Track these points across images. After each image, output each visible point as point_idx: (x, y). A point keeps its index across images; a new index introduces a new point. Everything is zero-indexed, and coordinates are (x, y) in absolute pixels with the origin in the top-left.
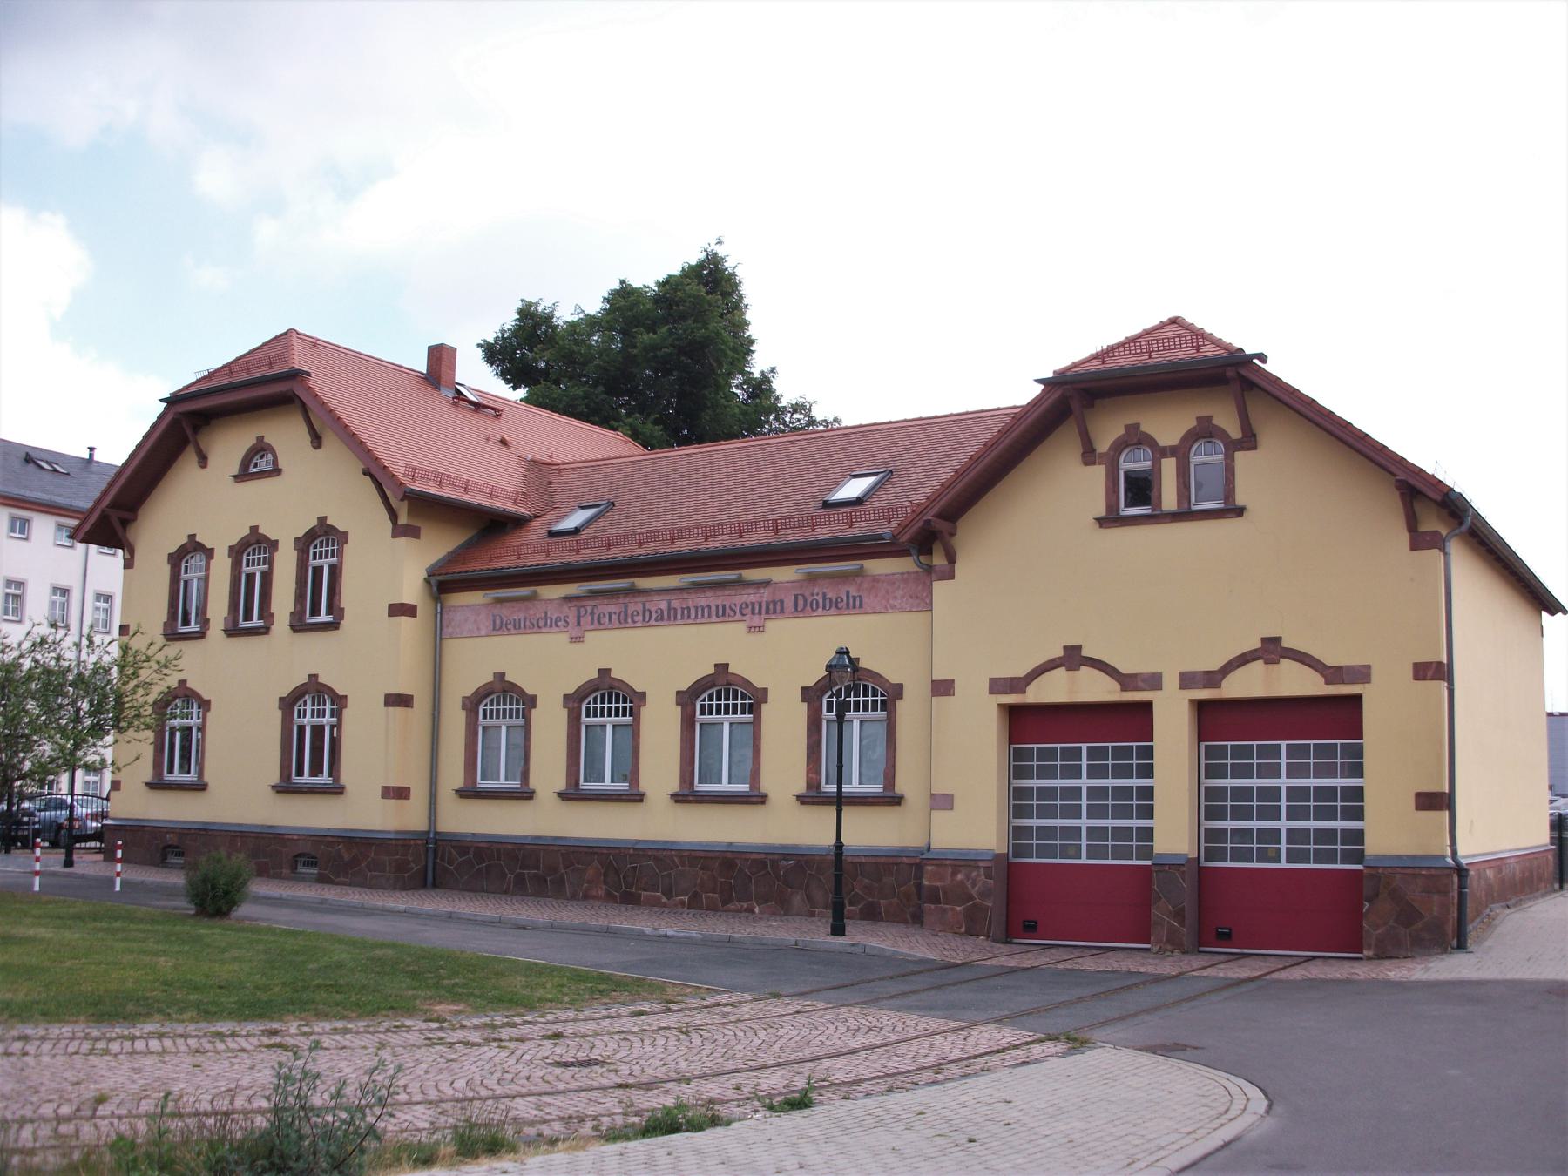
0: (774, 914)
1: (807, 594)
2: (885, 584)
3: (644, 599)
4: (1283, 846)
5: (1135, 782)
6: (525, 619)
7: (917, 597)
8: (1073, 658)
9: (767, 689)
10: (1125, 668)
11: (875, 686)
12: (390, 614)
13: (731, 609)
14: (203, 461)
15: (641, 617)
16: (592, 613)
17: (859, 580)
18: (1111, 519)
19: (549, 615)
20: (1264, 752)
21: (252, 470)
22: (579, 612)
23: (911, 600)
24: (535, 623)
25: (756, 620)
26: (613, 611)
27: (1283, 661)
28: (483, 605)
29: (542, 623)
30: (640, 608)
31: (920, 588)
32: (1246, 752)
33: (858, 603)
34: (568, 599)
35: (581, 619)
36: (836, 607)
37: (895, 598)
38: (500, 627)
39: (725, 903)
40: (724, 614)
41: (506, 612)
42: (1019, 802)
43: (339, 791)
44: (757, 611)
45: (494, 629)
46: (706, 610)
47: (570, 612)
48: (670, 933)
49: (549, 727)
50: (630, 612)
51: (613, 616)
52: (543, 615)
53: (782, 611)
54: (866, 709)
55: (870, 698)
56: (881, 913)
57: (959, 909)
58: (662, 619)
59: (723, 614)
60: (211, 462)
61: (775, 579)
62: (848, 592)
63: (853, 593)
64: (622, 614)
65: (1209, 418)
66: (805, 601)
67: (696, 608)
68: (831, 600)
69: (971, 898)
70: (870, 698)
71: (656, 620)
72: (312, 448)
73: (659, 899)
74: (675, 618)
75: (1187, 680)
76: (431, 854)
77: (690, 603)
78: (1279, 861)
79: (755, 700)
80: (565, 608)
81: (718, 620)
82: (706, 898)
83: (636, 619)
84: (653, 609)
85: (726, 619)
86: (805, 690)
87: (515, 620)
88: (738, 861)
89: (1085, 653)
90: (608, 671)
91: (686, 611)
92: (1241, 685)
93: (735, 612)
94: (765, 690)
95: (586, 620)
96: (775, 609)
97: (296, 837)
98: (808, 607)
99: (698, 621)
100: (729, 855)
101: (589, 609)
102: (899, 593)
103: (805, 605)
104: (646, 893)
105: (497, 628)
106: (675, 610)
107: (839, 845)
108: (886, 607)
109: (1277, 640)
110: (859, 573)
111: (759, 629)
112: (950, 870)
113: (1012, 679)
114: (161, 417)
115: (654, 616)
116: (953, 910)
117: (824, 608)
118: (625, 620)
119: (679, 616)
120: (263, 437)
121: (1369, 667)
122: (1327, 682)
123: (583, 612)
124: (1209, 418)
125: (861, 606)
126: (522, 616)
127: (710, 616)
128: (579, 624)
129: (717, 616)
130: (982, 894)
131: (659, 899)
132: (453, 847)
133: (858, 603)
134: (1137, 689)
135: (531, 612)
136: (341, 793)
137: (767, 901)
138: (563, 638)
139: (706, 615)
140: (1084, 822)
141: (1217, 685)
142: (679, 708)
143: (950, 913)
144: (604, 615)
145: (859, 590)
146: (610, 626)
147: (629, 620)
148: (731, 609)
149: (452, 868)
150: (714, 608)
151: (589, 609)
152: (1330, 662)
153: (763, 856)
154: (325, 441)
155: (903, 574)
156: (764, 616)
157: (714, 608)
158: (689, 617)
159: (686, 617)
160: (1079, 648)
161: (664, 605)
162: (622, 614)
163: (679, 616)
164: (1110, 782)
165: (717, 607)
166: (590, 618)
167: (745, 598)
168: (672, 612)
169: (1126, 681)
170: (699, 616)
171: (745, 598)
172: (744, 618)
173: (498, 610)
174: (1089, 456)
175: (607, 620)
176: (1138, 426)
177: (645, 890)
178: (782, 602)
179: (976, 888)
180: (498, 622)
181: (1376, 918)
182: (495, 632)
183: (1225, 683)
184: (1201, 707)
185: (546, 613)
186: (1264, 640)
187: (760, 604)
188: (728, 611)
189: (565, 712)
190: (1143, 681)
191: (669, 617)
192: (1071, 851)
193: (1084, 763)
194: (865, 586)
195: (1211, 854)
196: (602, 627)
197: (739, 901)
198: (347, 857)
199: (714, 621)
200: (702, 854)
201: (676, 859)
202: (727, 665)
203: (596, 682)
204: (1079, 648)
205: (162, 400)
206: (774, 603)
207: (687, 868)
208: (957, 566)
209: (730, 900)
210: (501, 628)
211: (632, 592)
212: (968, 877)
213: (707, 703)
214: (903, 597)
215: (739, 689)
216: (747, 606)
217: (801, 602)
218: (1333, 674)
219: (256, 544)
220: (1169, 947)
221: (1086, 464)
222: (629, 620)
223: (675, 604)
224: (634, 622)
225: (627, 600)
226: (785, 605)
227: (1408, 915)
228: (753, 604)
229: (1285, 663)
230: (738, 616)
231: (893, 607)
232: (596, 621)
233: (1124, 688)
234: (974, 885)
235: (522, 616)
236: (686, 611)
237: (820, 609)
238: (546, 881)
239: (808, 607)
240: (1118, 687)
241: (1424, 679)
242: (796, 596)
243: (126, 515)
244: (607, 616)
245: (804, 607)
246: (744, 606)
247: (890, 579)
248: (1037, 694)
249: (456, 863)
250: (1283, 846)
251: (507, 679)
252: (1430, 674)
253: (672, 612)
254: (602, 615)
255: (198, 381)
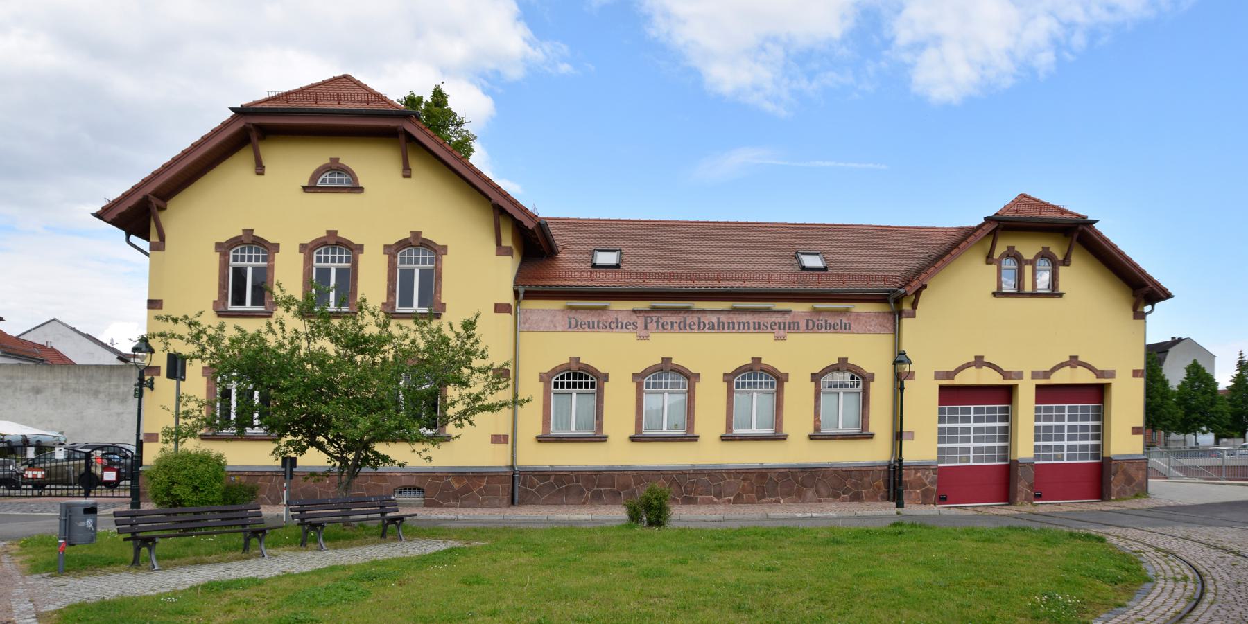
0: (795, 502)
1: (815, 320)
2: (865, 318)
3: (699, 315)
4: (1065, 453)
5: (947, 425)
6: (598, 322)
7: (884, 326)
8: (979, 362)
9: (812, 374)
10: (1005, 368)
11: (587, 374)
12: (496, 311)
13: (764, 325)
14: (260, 169)
15: (697, 327)
16: (657, 322)
17: (848, 314)
18: (998, 294)
19: (620, 320)
20: (1058, 410)
21: (319, 184)
22: (646, 320)
23: (880, 328)
24: (607, 325)
25: (781, 333)
26: (674, 321)
27: (1079, 367)
28: (559, 310)
29: (613, 326)
30: (696, 320)
31: (886, 321)
32: (1050, 410)
33: (847, 327)
34: (635, 311)
35: (646, 324)
36: (834, 328)
37: (871, 326)
38: (573, 326)
39: (759, 499)
40: (759, 328)
41: (581, 317)
42: (942, 435)
43: (603, 439)
44: (782, 328)
45: (570, 327)
46: (746, 325)
47: (640, 321)
48: (814, 515)
49: (711, 394)
50: (688, 323)
51: (675, 324)
52: (614, 320)
53: (798, 328)
54: (581, 387)
55: (578, 381)
56: (862, 497)
57: (918, 491)
58: (713, 328)
59: (758, 328)
60: (267, 170)
61: (793, 310)
62: (841, 320)
63: (845, 320)
64: (682, 324)
65: (1048, 248)
66: (577, 322)
67: (739, 323)
68: (830, 324)
69: (925, 485)
70: (578, 381)
71: (709, 329)
72: (402, 176)
73: (712, 499)
74: (723, 329)
75: (1035, 375)
76: (892, 475)
77: (734, 320)
78: (1063, 460)
79: (779, 379)
80: (634, 318)
81: (755, 331)
82: (746, 497)
83: (665, 327)
84: (706, 322)
85: (761, 331)
86: (813, 375)
87: (589, 322)
88: (769, 474)
89: (985, 360)
90: (670, 359)
91: (731, 325)
92: (962, 379)
93: (767, 328)
94: (787, 374)
95: (652, 326)
96: (794, 327)
97: (399, 474)
98: (816, 328)
99: (740, 331)
100: (764, 471)
101: (655, 319)
102: (873, 323)
103: (814, 326)
104: (701, 497)
105: (573, 326)
106: (723, 323)
107: (512, 467)
108: (865, 330)
109: (1076, 357)
110: (604, 309)
111: (783, 338)
112: (913, 471)
113: (947, 372)
114: (225, 125)
115: (707, 326)
116: (915, 492)
117: (826, 328)
118: (683, 327)
119: (726, 328)
120: (339, 159)
121: (1114, 371)
122: (1097, 378)
123: (649, 320)
124: (1048, 248)
125: (850, 329)
126: (595, 320)
127: (749, 329)
128: (646, 328)
129: (754, 328)
130: (931, 483)
131: (712, 499)
132: (533, 476)
133: (847, 327)
134: (1010, 378)
135: (604, 318)
136: (605, 441)
137: (789, 495)
138: (633, 337)
139: (746, 328)
140: (1066, 443)
141: (1049, 378)
142: (726, 384)
143: (913, 494)
144: (667, 323)
145: (848, 319)
146: (672, 331)
147: (688, 328)
148: (764, 325)
149: (533, 490)
150: (752, 325)
151: (655, 319)
152: (1099, 368)
153: (788, 470)
154: (414, 173)
155: (876, 313)
156: (787, 331)
157: (752, 325)
158: (734, 328)
159: (731, 328)
160: (982, 357)
161: (714, 320)
162: (682, 324)
163: (726, 328)
164: (1079, 423)
165: (754, 323)
166: (655, 324)
167: (773, 319)
168: (721, 324)
169: (1005, 375)
170: (741, 328)
171: (773, 319)
172: (774, 331)
173: (572, 314)
174: (989, 259)
175: (669, 326)
176: (1013, 247)
177: (701, 495)
178: (798, 323)
179: (928, 480)
180: (573, 323)
181: (1116, 482)
182: (569, 330)
183: (1052, 377)
184: (942, 388)
185: (617, 319)
186: (1071, 357)
187: (784, 323)
188: (762, 326)
189: (635, 384)
190: (1014, 374)
191: (719, 327)
192: (964, 459)
193: (972, 415)
194: (852, 317)
195: (941, 460)
196: (666, 331)
197: (770, 497)
198: (456, 486)
199: (750, 331)
200: (744, 471)
201: (724, 474)
202: (760, 359)
203: (660, 366)
204: (982, 357)
205: (232, 109)
206: (794, 323)
207: (733, 480)
208: (917, 310)
209: (764, 497)
210: (576, 326)
211: (687, 310)
212: (924, 474)
213: (559, 381)
214: (875, 325)
215: (584, 373)
216: (775, 324)
217: (811, 325)
218: (1100, 374)
219: (333, 243)
220: (1026, 502)
221: (987, 263)
222: (688, 328)
223: (722, 319)
224: (692, 329)
225: (686, 315)
226: (800, 325)
227: (1129, 480)
228: (780, 323)
229: (985, 368)
230: (769, 330)
231: (870, 330)
232: (660, 327)
233: (1098, 377)
234: (927, 479)
235: (595, 320)
236: (731, 325)
237: (823, 329)
238: (620, 494)
239: (816, 328)
240: (1002, 377)
241: (1137, 377)
242: (808, 321)
243: (160, 203)
244: (670, 324)
245: (811, 327)
246: (773, 324)
247: (868, 315)
248: (959, 380)
249: (537, 486)
250: (1065, 453)
251: (581, 361)
252: (1140, 374)
253: (721, 324)
254: (665, 323)
255: (269, 100)
